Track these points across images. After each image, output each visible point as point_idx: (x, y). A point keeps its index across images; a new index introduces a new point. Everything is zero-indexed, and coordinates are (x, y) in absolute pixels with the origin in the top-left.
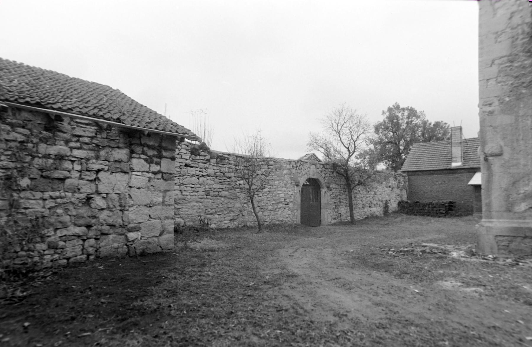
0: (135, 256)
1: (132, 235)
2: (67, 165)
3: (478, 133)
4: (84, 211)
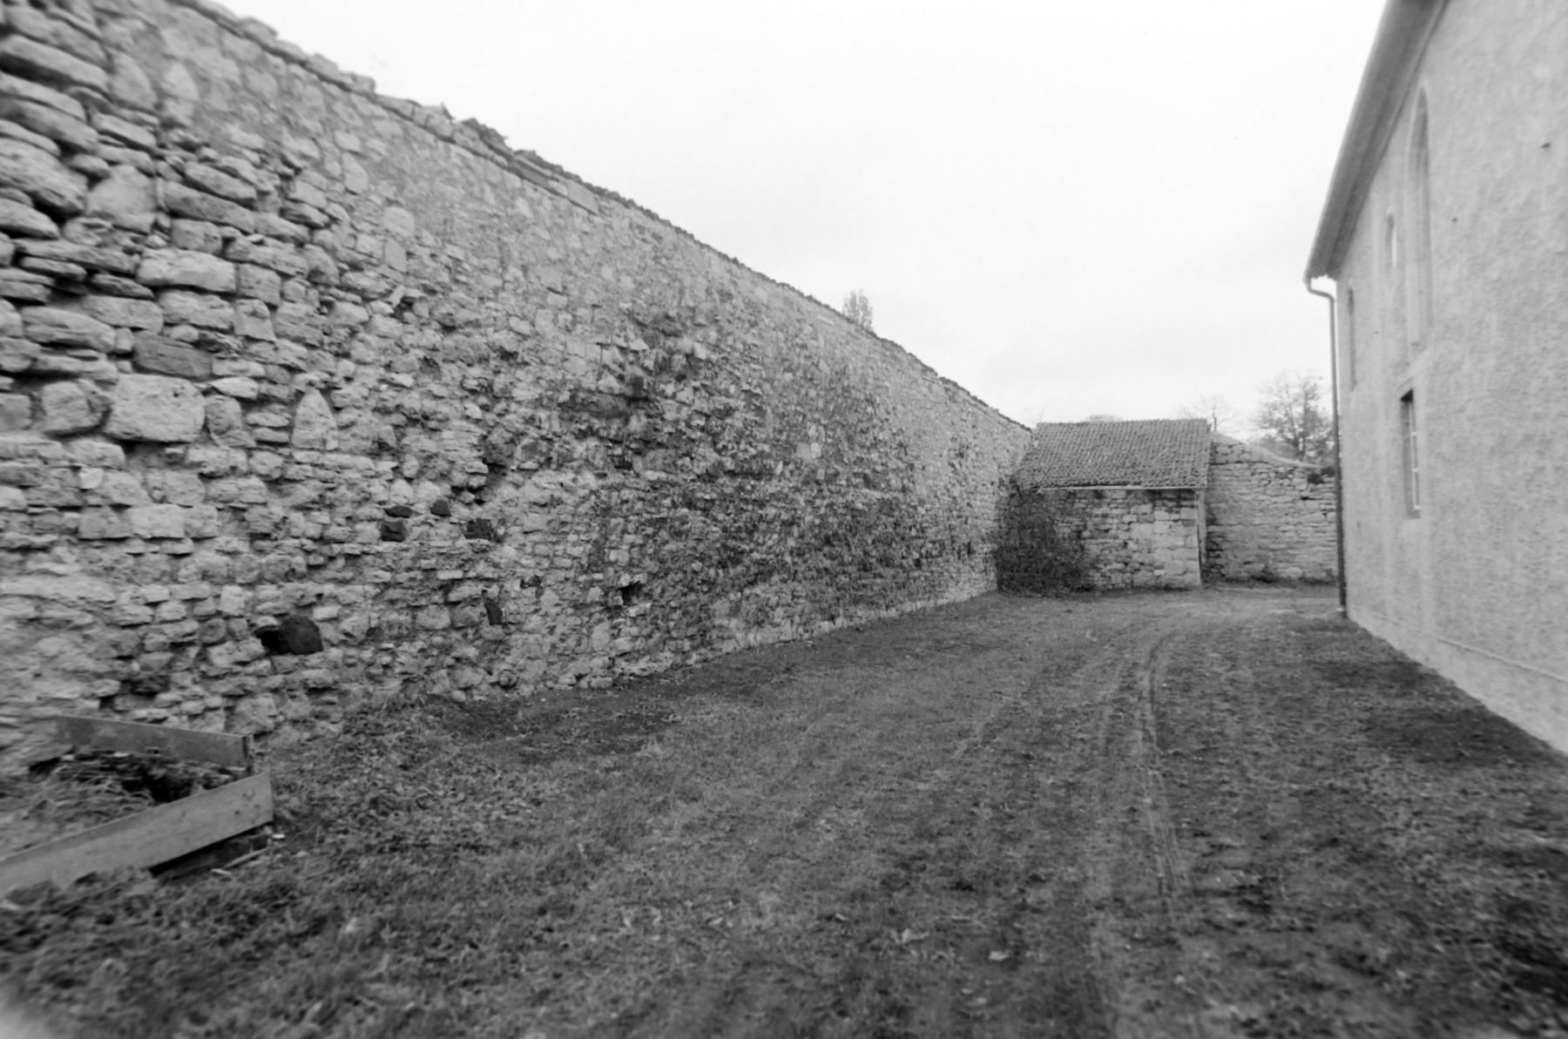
0: (630, 685)
1: (1157, 572)
2: (1109, 520)
3: (855, 320)
4: (1123, 553)
